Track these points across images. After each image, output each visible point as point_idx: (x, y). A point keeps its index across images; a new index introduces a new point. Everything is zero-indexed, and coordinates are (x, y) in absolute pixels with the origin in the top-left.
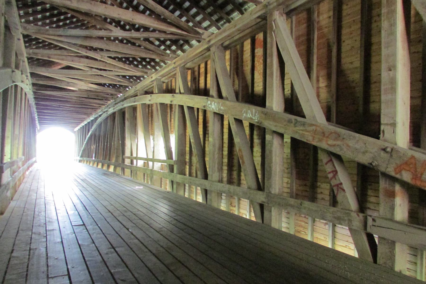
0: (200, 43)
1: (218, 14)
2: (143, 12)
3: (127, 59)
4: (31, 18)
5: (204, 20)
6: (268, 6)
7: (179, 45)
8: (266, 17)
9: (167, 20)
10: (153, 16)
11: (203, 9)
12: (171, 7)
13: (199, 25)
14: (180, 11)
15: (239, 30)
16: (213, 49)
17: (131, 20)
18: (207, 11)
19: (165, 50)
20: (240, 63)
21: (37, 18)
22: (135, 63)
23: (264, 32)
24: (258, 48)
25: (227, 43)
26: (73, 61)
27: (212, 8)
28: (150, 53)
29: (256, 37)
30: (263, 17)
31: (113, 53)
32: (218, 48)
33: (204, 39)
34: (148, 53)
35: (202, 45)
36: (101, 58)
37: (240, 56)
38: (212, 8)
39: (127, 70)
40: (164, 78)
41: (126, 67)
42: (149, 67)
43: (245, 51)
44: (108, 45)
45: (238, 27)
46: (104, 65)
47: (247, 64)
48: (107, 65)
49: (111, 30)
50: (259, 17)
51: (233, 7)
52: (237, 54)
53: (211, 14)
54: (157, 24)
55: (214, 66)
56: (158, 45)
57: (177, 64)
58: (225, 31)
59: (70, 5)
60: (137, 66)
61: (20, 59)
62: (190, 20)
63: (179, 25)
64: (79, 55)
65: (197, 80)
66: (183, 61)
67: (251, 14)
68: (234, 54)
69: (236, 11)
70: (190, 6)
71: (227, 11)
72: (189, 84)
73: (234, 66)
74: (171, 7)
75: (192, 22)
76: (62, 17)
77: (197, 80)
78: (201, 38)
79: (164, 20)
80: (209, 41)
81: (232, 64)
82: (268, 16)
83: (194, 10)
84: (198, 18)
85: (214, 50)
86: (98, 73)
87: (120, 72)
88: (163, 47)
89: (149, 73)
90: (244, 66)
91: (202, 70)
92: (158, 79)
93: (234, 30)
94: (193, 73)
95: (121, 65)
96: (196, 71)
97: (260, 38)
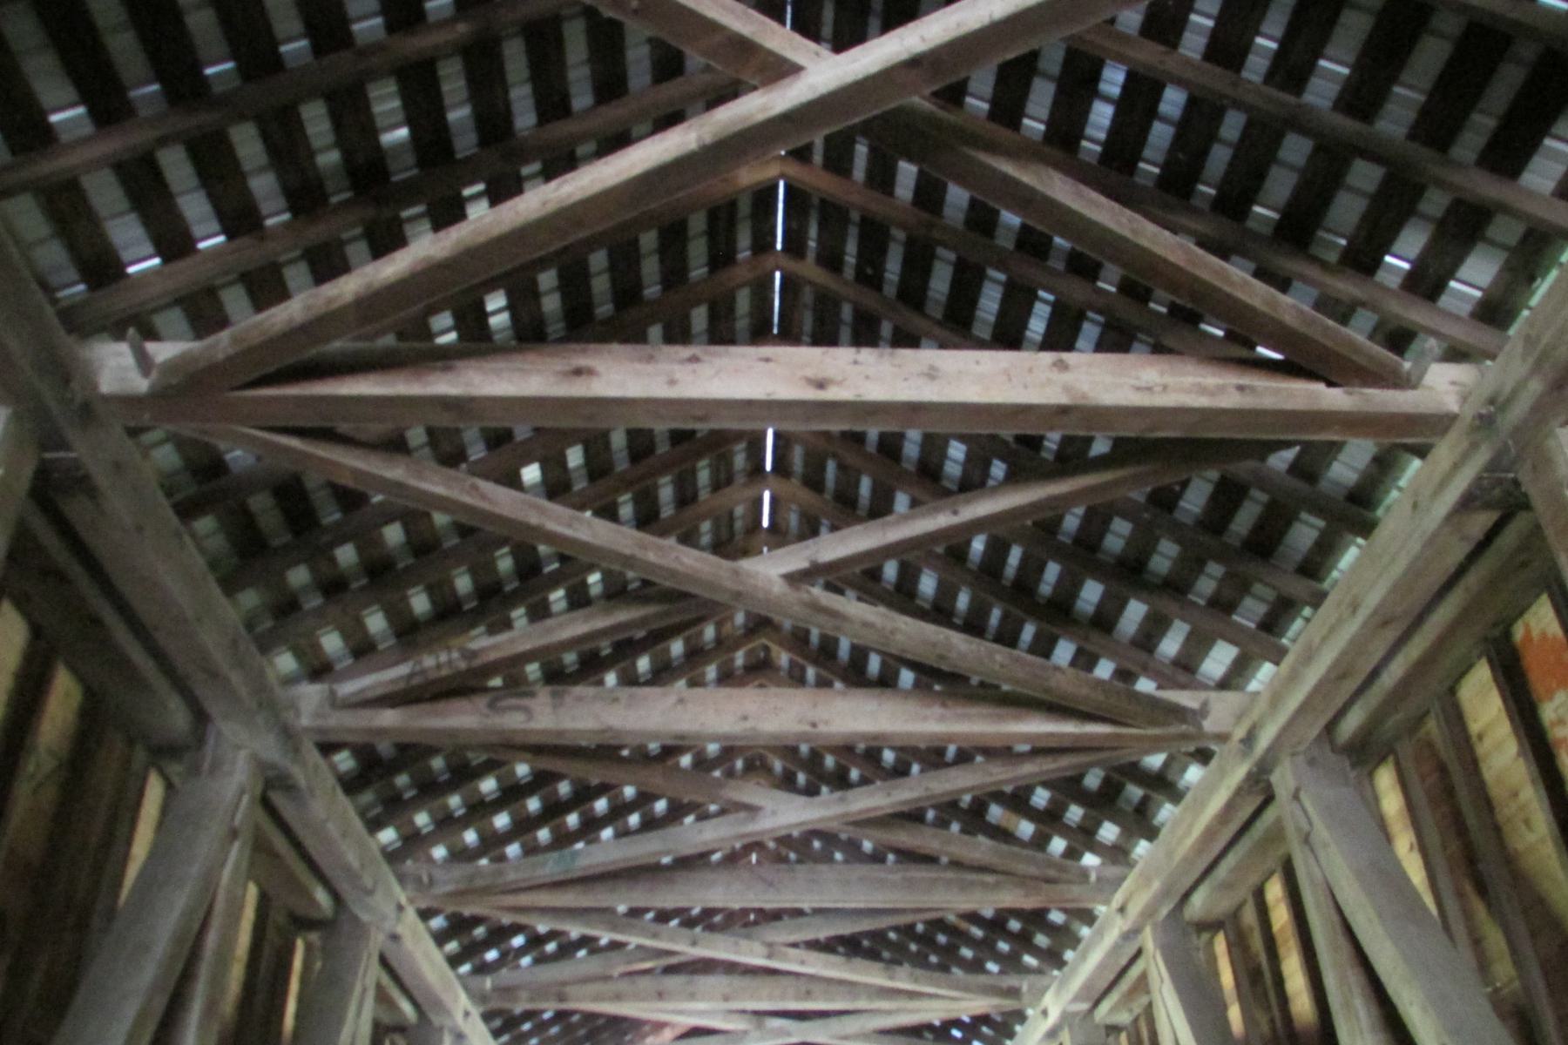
0: (1214, 763)
1: (1258, 588)
2: (886, 682)
3: (878, 936)
4: (470, 837)
5: (1198, 645)
6: (1499, 420)
7: (1129, 809)
8: (1516, 483)
9: (997, 687)
10: (937, 688)
11: (1176, 587)
12: (1028, 632)
13: (1182, 677)
14: (1071, 637)
15: (1385, 623)
16: (1283, 779)
17: (807, 728)
18: (1200, 596)
19: (1072, 854)
20: (1472, 821)
21: (495, 832)
22: (967, 953)
23: (1548, 588)
24: (1550, 695)
25: (1352, 722)
26: (660, 995)
27: (1215, 569)
28: (985, 885)
29: (1518, 632)
30: (1497, 492)
31: (818, 920)
32: (1312, 762)
33: (1223, 738)
34: (972, 883)
35: (1222, 773)
36: (770, 956)
37: (1455, 769)
38: (1215, 569)
39: (912, 995)
40: (1105, 1006)
41: (903, 979)
42: (1029, 960)
43: (1480, 737)
44: (771, 884)
45: (1373, 599)
46: (803, 989)
47: (1522, 808)
48: (816, 988)
49: (752, 810)
50: (1467, 503)
51: (1321, 523)
52: (1443, 769)
53: (1223, 605)
54: (942, 719)
55: (1316, 870)
56: (1034, 836)
57: (1134, 910)
58: (1308, 657)
59: (523, 726)
60: (976, 966)
61: (441, 1029)
62: (1133, 668)
63: (1047, 691)
64: (673, 960)
65: (1268, 975)
66: (1156, 885)
67: (1415, 506)
68: (1423, 778)
69: (1350, 537)
70: (1105, 596)
71: (1299, 558)
72: (1235, 1014)
73: (1445, 848)
74: (1028, 632)
75: (1147, 670)
76: (601, 805)
77: (1268, 975)
78: (1201, 734)
79: (991, 695)
80: (1249, 740)
81: (1434, 839)
82: (1524, 475)
83: (1135, 612)
84: (1170, 645)
85: (1291, 784)
86: (789, 1034)
87: (889, 1013)
88: (1058, 845)
89: (1025, 988)
90: (1506, 829)
91: (1281, 916)
92: (1075, 1014)
93: (1352, 627)
94: (1239, 945)
95: (870, 975)
96: (1251, 929)
97: (1544, 635)
